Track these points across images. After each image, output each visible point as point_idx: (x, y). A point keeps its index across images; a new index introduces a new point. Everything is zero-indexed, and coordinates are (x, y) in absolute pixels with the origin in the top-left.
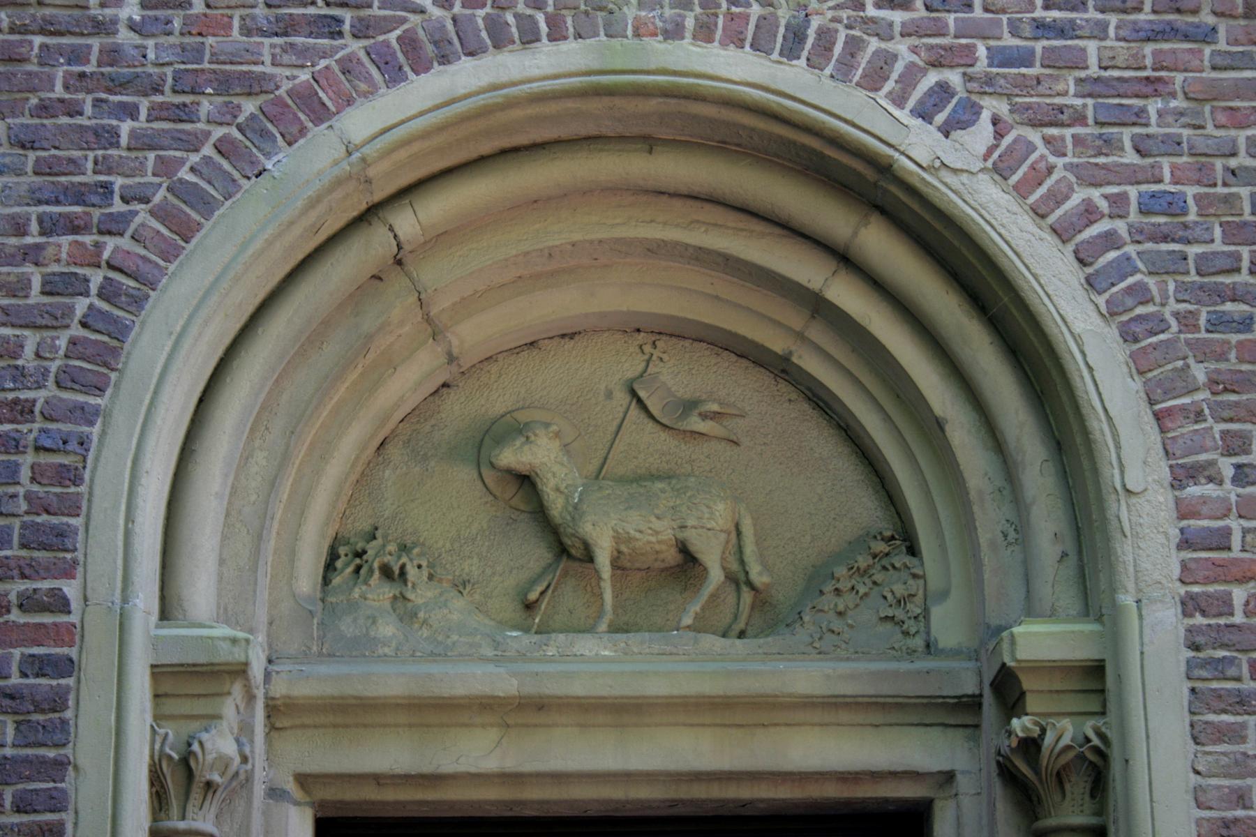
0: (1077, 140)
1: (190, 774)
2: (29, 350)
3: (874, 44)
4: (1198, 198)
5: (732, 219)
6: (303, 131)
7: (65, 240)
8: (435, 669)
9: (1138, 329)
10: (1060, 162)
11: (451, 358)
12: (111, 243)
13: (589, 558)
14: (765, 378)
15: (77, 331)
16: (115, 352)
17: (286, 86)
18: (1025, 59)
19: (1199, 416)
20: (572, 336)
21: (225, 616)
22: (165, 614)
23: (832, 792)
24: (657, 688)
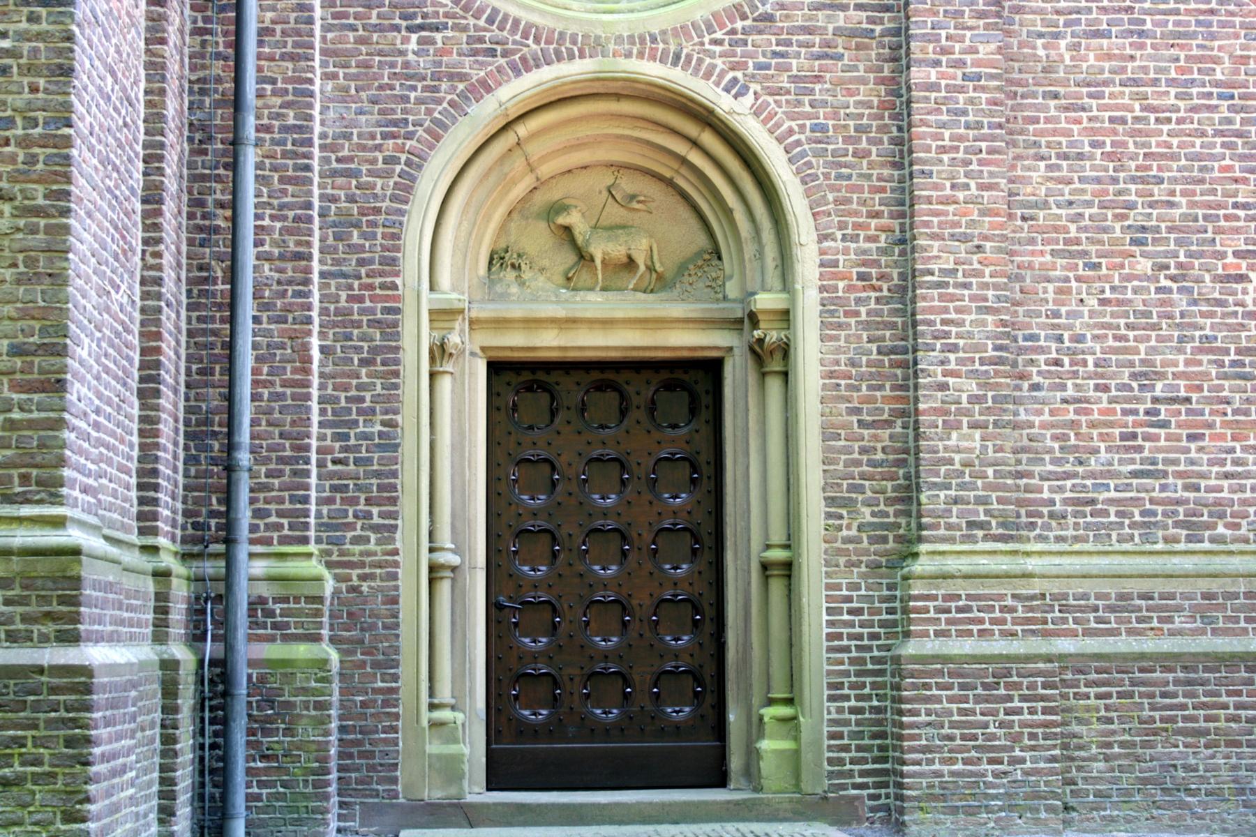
0: (787, 102)
1: (444, 350)
2: (379, 187)
3: (708, 60)
4: (834, 126)
5: (650, 126)
6: (482, 97)
7: (391, 142)
8: (534, 306)
9: (807, 179)
10: (780, 110)
11: (538, 179)
12: (409, 143)
13: (592, 260)
14: (663, 186)
15: (397, 179)
16: (412, 188)
17: (475, 78)
18: (768, 67)
19: (829, 214)
20: (585, 168)
21: (454, 290)
22: (432, 289)
23: (686, 354)
24: (619, 314)
